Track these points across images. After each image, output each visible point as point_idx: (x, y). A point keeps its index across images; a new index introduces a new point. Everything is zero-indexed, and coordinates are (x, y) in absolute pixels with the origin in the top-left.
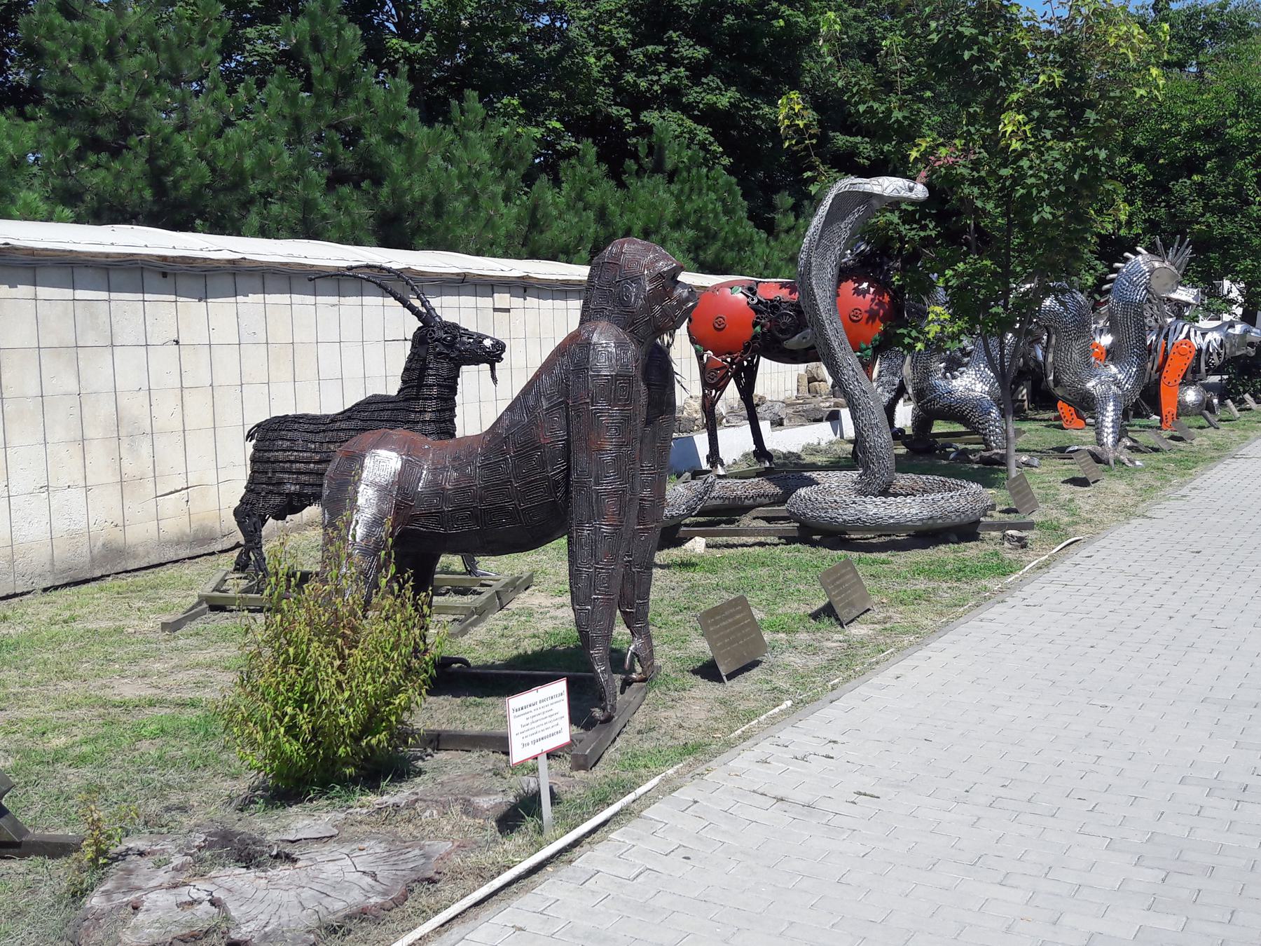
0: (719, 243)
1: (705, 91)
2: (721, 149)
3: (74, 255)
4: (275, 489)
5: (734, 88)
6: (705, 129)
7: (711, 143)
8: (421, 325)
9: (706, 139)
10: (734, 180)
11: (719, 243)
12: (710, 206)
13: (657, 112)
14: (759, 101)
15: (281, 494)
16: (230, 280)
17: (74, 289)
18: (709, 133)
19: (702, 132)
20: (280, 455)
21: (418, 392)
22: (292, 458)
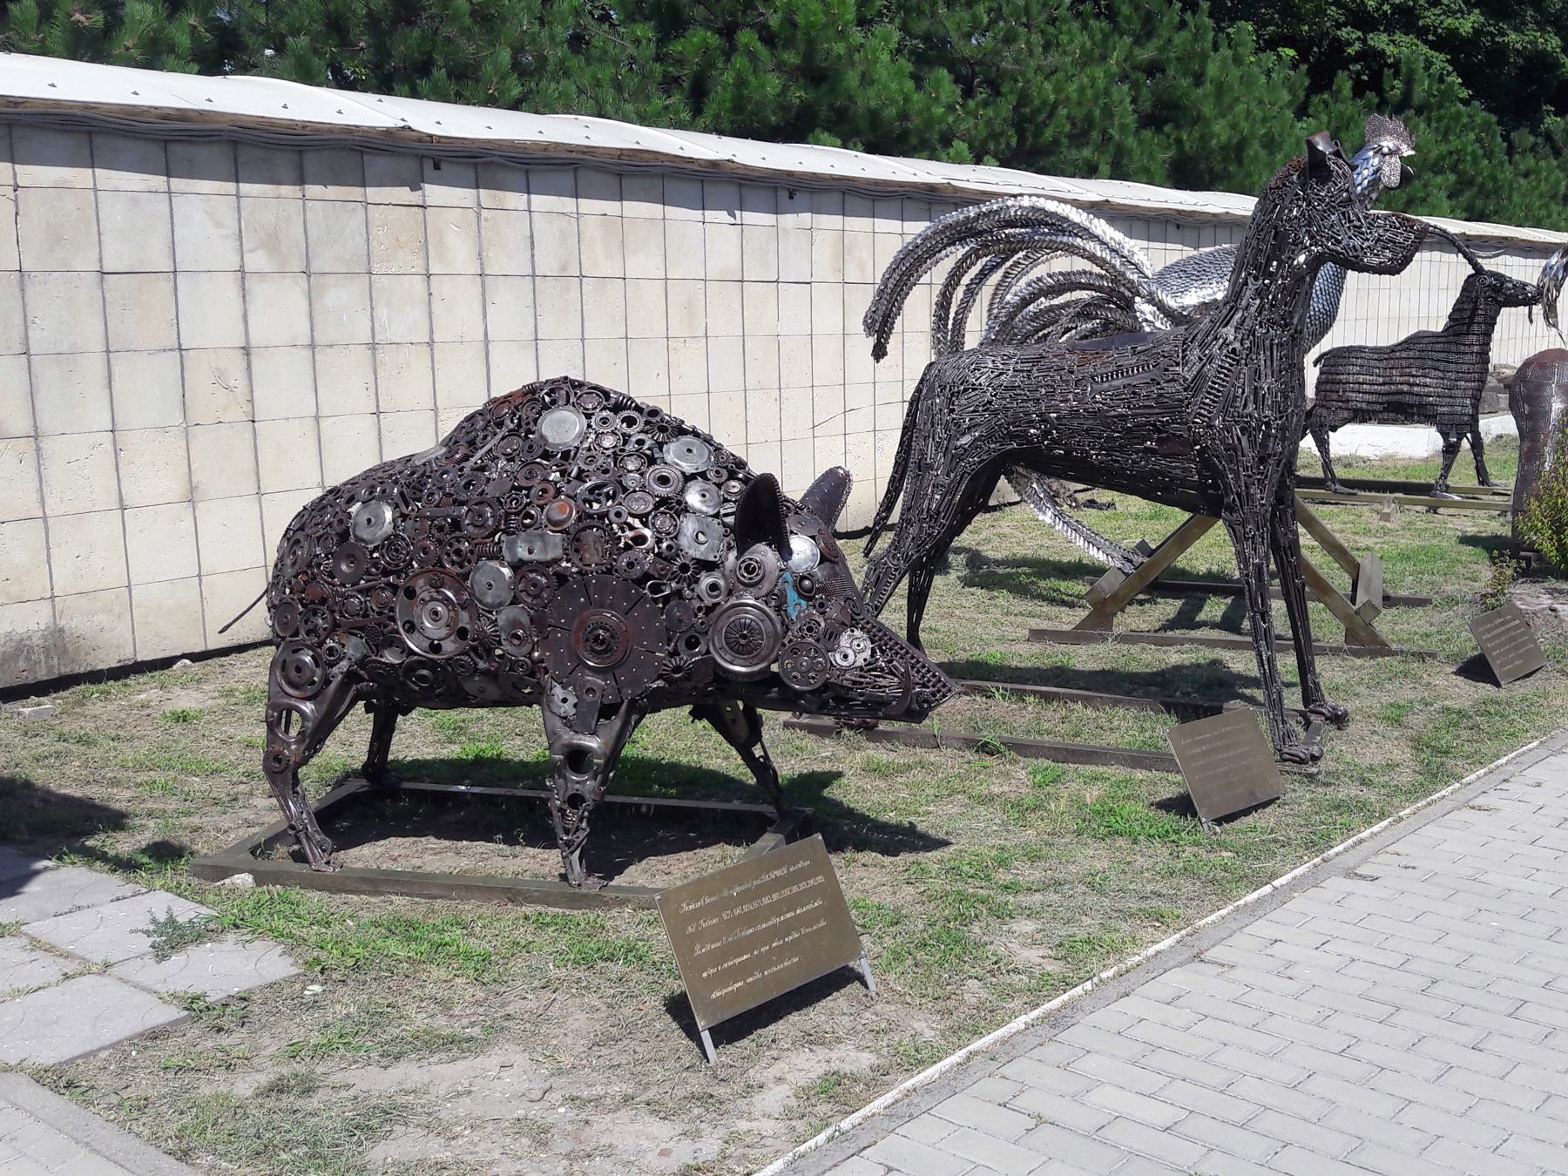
0: (1475, 189)
1: (1444, 13)
2: (1460, 80)
3: (478, 145)
4: (1344, 406)
5: (1477, 11)
6: (1442, 57)
7: (1449, 74)
8: (1473, 272)
9: (1443, 69)
10: (1494, 118)
11: (1475, 189)
12: (1470, 149)
13: (1385, 34)
14: (1505, 27)
15: (1347, 409)
16: (697, 187)
17: (237, 182)
18: (1447, 61)
19: (1440, 60)
20: (1351, 379)
21: (1468, 329)
22: (1361, 380)
